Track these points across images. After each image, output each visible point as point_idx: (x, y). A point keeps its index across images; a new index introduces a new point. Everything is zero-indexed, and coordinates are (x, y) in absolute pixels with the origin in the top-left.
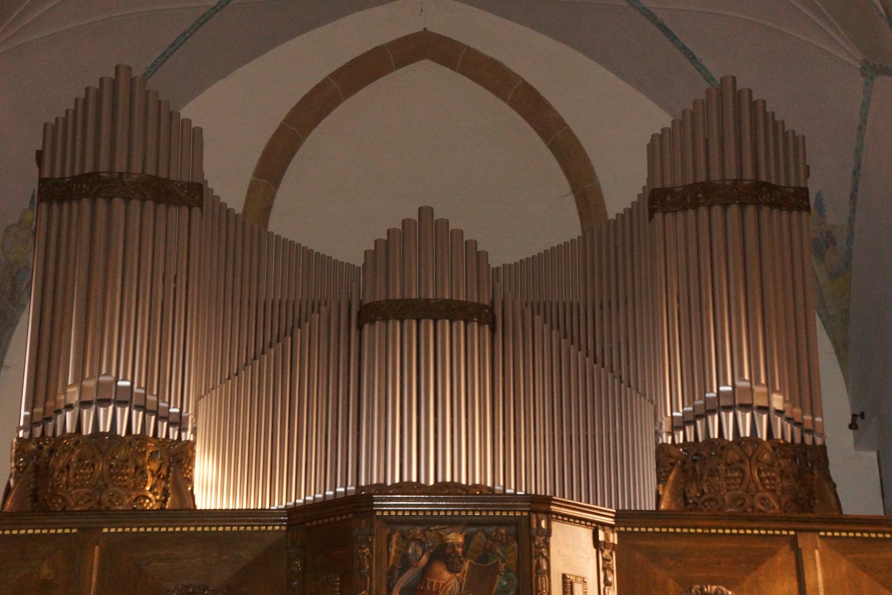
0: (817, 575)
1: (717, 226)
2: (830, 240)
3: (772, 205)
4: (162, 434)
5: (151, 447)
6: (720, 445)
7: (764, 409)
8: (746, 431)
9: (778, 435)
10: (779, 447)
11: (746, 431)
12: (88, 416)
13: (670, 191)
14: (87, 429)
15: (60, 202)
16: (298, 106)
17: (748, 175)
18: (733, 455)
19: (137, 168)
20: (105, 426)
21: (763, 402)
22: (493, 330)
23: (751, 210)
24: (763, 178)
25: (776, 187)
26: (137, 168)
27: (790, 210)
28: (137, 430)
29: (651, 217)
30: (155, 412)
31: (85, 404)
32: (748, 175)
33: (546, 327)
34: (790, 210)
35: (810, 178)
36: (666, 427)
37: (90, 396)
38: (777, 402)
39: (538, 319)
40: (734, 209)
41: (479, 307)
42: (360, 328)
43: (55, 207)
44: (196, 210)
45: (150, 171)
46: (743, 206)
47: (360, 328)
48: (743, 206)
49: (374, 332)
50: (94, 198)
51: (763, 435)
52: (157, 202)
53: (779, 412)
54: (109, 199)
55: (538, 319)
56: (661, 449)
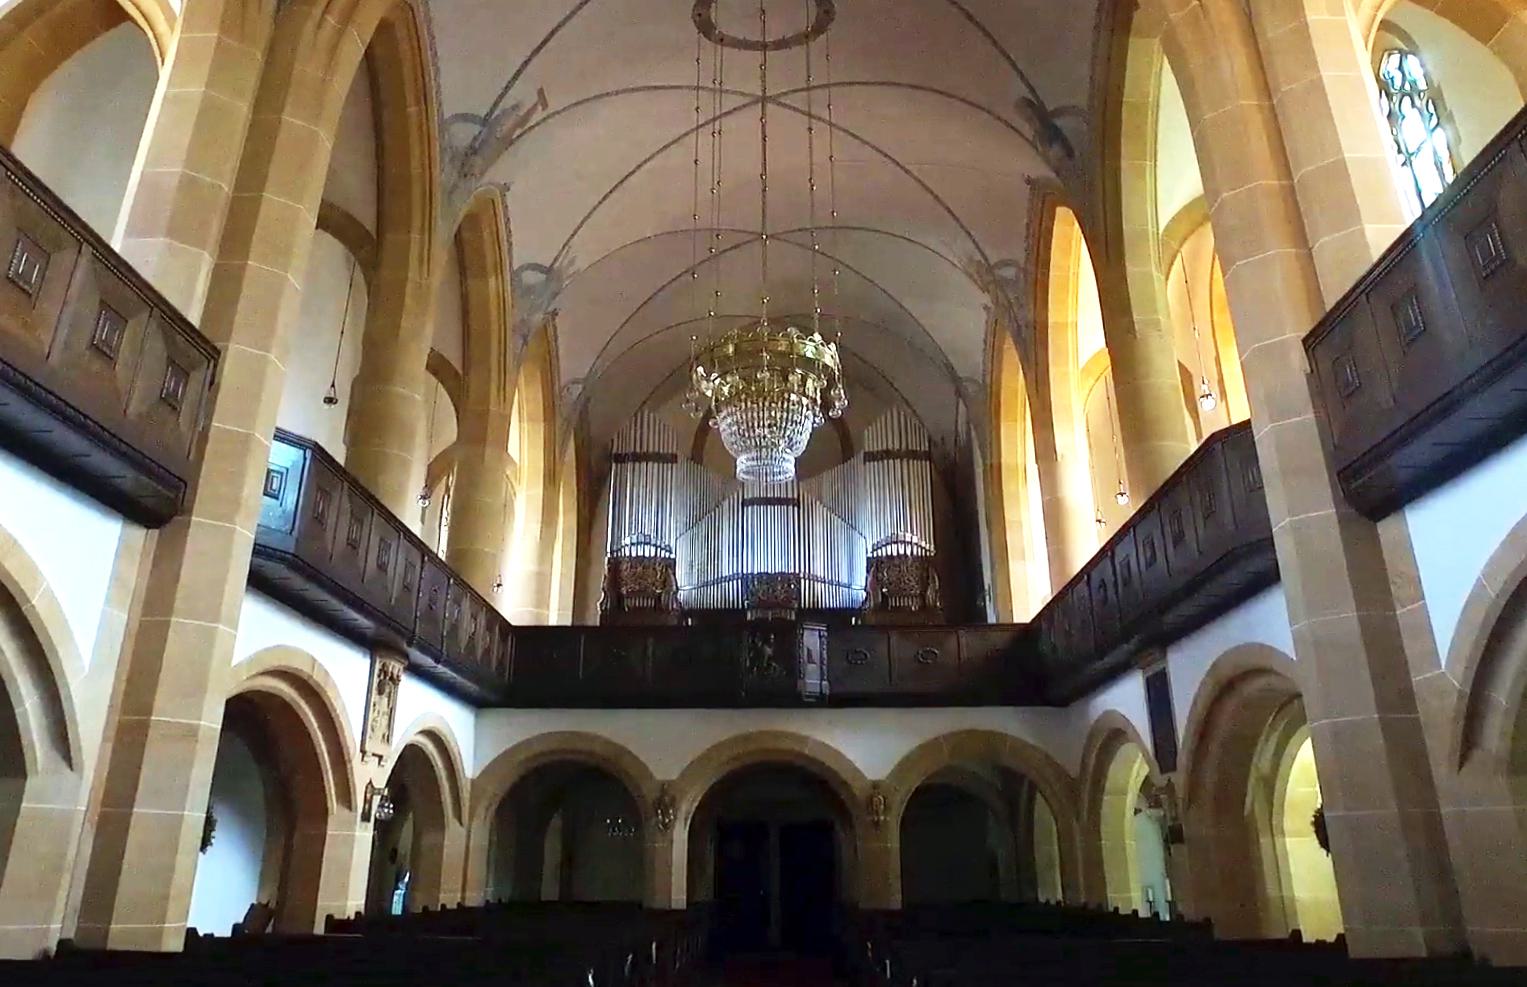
0: (1123, 500)
1: (656, 470)
4: (663, 555)
5: (659, 560)
6: (890, 557)
8: (902, 552)
9: (915, 553)
10: (916, 558)
11: (902, 552)
15: (621, 462)
18: (897, 562)
20: (640, 553)
21: (909, 540)
28: (653, 554)
29: (865, 463)
31: (632, 544)
36: (870, 550)
37: (634, 541)
38: (915, 540)
39: (818, 503)
40: (898, 461)
43: (661, 465)
44: (674, 465)
52: (914, 459)
53: (916, 544)
54: (640, 462)
55: (818, 503)
56: (868, 559)
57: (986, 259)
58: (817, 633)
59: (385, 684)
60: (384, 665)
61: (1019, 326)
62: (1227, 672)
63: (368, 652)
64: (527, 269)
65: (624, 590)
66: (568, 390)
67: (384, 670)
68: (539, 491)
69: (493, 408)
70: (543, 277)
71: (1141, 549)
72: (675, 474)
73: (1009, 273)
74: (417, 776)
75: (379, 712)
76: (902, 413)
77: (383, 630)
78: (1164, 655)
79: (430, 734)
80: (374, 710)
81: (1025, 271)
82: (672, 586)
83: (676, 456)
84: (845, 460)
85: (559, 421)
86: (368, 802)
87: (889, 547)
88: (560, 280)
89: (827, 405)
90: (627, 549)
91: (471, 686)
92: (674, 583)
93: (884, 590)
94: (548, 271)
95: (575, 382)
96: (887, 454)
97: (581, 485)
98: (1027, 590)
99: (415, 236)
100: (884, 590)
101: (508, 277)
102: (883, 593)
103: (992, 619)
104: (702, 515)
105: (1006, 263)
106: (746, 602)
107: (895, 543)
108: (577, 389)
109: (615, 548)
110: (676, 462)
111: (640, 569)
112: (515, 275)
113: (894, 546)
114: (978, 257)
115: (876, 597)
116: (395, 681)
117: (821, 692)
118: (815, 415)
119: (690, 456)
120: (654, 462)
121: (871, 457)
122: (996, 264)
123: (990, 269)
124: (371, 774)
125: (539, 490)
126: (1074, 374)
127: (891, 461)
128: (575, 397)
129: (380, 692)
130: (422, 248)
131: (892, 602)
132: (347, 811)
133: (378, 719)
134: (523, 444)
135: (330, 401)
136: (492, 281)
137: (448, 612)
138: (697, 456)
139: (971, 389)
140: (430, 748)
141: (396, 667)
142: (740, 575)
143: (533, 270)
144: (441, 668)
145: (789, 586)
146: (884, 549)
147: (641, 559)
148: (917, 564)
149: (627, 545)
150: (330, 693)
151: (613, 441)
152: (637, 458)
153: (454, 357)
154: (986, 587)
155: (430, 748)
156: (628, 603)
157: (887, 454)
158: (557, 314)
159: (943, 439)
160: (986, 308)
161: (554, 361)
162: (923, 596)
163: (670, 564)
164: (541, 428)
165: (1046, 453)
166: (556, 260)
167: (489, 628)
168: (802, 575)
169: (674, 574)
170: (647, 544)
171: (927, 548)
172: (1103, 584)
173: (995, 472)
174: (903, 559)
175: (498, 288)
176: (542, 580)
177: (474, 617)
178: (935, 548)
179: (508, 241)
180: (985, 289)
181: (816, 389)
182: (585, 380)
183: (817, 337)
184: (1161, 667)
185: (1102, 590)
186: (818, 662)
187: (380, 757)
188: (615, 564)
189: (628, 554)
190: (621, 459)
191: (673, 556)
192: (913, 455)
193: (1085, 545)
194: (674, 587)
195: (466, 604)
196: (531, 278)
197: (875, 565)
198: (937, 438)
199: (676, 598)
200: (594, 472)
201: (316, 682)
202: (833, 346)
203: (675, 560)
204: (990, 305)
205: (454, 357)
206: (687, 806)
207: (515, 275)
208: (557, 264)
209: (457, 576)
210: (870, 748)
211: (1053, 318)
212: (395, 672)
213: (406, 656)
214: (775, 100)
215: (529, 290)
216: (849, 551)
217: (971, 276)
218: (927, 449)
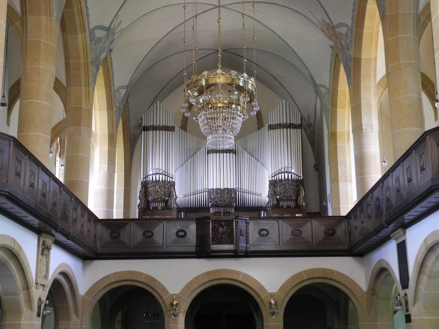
2: (311, 125)
3: (294, 128)
4: (168, 180)
6: (281, 181)
7: (291, 172)
9: (293, 178)
12: (154, 176)
13: (272, 125)
14: (154, 180)
15: (147, 131)
16: (284, 317)
17: (288, 122)
19: (285, 122)
22: (236, 154)
23: (289, 129)
24: (291, 122)
25: (294, 124)
26: (161, 124)
27: (297, 129)
30: (167, 175)
31: (153, 174)
32: (288, 122)
33: (247, 153)
34: (297, 129)
35: (351, 16)
36: (271, 176)
37: (154, 173)
41: (233, 150)
42: (208, 155)
45: (164, 125)
46: (287, 129)
47: (208, 155)
48: (287, 129)
49: (211, 155)
50: (153, 130)
51: (290, 178)
57: (332, 23)
58: (244, 221)
59: (44, 250)
60: (44, 242)
61: (347, 60)
62: (430, 243)
63: (37, 235)
64: (121, 89)
65: (150, 198)
66: (118, 92)
67: (44, 244)
68: (106, 148)
69: (84, 106)
70: (105, 33)
71: (405, 172)
72: (174, 137)
73: (343, 30)
74: (60, 291)
75: (42, 264)
76: (288, 104)
77: (43, 224)
78: (405, 233)
79: (64, 274)
80: (40, 264)
81: (351, 31)
82: (173, 195)
83: (174, 127)
84: (259, 128)
85: (115, 109)
86: (39, 307)
87: (280, 175)
88: (113, 33)
89: (250, 109)
90: (151, 177)
91: (80, 249)
92: (175, 194)
93: (277, 197)
94: (108, 29)
95: (122, 87)
96: (281, 126)
97: (126, 143)
98: (347, 197)
99: (83, 88)
100: (277, 197)
101: (87, 33)
102: (277, 199)
103: (330, 214)
104: (189, 157)
105: (342, 25)
106: (210, 204)
107: (283, 173)
108: (123, 92)
109: (145, 177)
110: (174, 131)
111: (158, 187)
112: (92, 32)
113: (283, 175)
114: (327, 21)
115: (273, 201)
116: (49, 249)
117: (246, 250)
118: (244, 115)
119: (180, 126)
120: (163, 130)
121: (272, 127)
122: (336, 25)
123: (333, 28)
124: (40, 294)
125: (106, 148)
126: (373, 85)
127: (282, 129)
128: (122, 96)
129: (42, 254)
130: (86, 97)
131: (281, 203)
132: (30, 311)
133: (42, 268)
134: (99, 121)
135: (3, 105)
136: (80, 35)
137: (72, 214)
138: (184, 127)
139: (323, 90)
140: (62, 280)
141: (49, 241)
142: (207, 190)
143: (100, 29)
144: (69, 242)
145: (231, 195)
146: (278, 176)
147: (157, 182)
148: (294, 184)
149: (150, 175)
150: (22, 256)
151: (142, 119)
152: (155, 128)
153: (63, 81)
154: (328, 196)
155: (62, 280)
156: (152, 205)
157: (281, 126)
158: (112, 51)
159: (308, 117)
160: (331, 47)
161: (111, 77)
162: (296, 200)
163: (173, 184)
164: (105, 113)
165: (358, 129)
166: (111, 24)
167: (89, 221)
168: (237, 190)
169: (174, 189)
170: (161, 174)
171: (299, 175)
172: (378, 199)
173: (333, 136)
174: (287, 181)
175: (83, 40)
176: (109, 194)
177: (83, 216)
178: (303, 175)
179: (85, 6)
180: (330, 39)
181: (244, 102)
182: (127, 86)
183: (245, 75)
184: (403, 240)
185: (377, 201)
186: (245, 235)
187: (43, 286)
188: (145, 185)
189: (151, 179)
190: (146, 129)
191: (173, 180)
192: (295, 127)
193: (375, 175)
194: (175, 196)
195: (79, 209)
196: (99, 33)
197: (273, 184)
198: (305, 116)
199: (176, 202)
200: (133, 133)
201: (16, 251)
202: (252, 79)
203: (174, 182)
204: (333, 45)
205: (63, 81)
206: (184, 307)
207: (92, 32)
208: (112, 26)
209: (71, 196)
210: (270, 277)
211: (364, 56)
212: (49, 245)
213: (53, 236)
214: (223, 6)
215: (99, 40)
216: (259, 175)
217: (323, 31)
218: (300, 123)
